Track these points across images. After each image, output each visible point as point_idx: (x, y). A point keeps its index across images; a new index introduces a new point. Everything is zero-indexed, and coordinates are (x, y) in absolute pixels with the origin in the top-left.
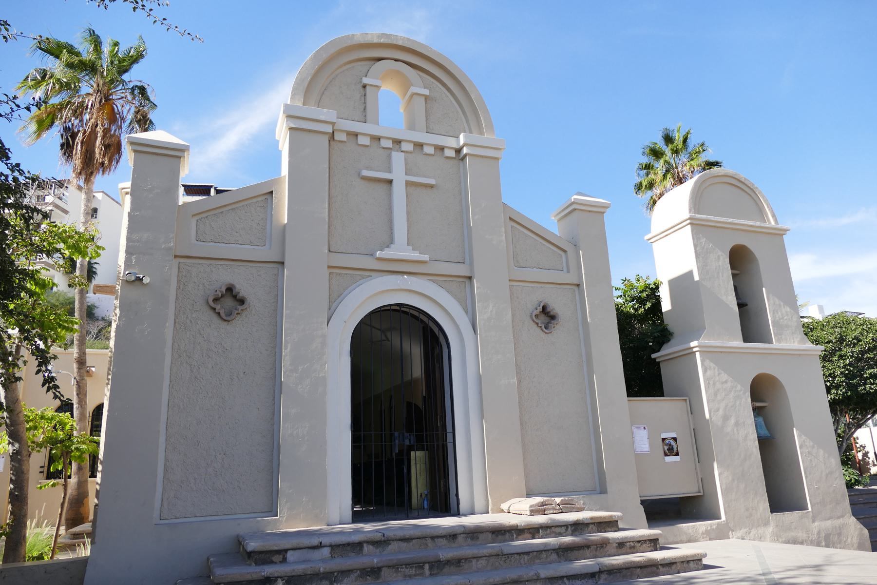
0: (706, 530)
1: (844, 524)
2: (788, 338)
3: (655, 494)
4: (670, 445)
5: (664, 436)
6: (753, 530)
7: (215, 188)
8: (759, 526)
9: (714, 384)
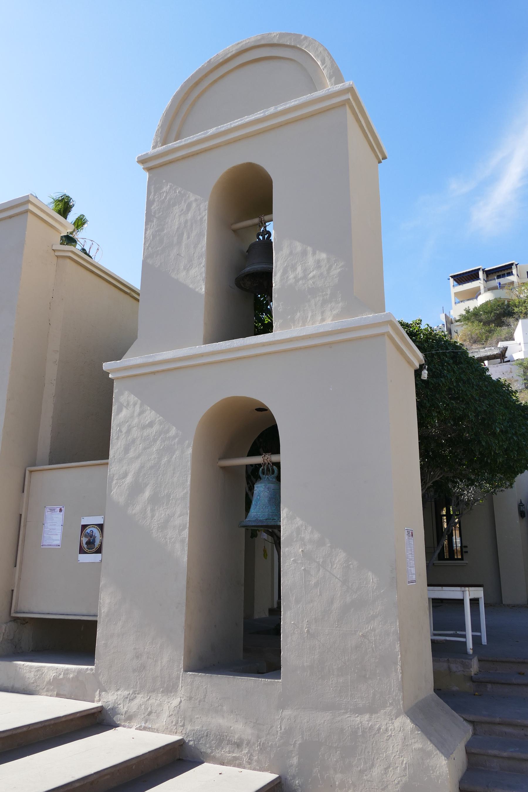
0: (55, 678)
1: (371, 728)
2: (310, 315)
3: (55, 611)
4: (91, 536)
5: (85, 521)
6: (140, 696)
7: (483, 270)
8: (153, 690)
9: (129, 431)
